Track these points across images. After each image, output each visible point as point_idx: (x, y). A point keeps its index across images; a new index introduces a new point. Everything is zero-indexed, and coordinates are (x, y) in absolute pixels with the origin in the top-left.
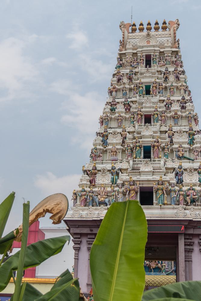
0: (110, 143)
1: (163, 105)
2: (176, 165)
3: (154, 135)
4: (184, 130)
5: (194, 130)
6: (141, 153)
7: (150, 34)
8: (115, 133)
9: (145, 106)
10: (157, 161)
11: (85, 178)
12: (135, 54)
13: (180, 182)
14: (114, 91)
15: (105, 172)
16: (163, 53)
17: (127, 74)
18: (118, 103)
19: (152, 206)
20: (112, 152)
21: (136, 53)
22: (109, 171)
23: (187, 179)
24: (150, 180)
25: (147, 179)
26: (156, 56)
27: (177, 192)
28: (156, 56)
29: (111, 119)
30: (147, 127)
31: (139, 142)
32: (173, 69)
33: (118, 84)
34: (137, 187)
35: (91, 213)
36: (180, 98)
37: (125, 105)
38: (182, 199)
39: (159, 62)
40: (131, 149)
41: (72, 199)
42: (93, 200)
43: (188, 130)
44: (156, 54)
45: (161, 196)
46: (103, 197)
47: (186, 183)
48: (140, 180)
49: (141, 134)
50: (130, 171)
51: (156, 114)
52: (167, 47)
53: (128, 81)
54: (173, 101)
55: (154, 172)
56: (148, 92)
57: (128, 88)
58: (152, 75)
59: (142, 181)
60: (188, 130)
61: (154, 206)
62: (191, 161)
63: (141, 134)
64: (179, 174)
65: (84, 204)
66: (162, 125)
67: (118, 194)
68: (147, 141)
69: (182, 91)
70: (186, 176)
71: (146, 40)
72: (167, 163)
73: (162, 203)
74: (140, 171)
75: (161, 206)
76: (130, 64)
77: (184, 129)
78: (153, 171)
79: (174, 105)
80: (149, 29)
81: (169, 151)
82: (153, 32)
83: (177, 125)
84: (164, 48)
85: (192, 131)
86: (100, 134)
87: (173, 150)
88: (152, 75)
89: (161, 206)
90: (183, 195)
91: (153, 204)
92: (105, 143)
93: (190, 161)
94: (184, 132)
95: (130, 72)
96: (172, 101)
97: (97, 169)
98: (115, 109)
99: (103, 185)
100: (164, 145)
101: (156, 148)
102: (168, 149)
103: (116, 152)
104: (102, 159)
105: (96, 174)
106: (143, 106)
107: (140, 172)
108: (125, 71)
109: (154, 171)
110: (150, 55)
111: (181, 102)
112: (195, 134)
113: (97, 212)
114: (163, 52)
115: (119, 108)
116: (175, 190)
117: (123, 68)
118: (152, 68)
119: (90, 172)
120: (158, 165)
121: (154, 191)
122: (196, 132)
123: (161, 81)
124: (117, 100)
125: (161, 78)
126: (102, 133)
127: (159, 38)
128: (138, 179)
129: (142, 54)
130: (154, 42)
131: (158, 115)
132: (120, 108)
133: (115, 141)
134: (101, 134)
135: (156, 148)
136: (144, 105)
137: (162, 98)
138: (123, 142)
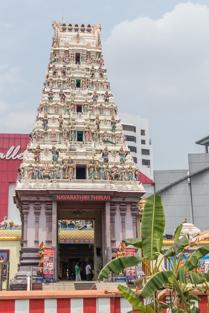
25: (82, 159)
43: (110, 119)
44: (84, 53)
52: (92, 48)
59: (79, 160)
60: (110, 119)
61: (87, 180)
68: (80, 127)
74: (76, 151)
93: (113, 144)
96: (98, 94)
103: (55, 135)
114: (89, 52)
120: (90, 147)
122: (117, 121)
124: (54, 91)
125: (88, 74)
126: (43, 118)
128: (75, 159)
136: (76, 96)
137: (90, 92)
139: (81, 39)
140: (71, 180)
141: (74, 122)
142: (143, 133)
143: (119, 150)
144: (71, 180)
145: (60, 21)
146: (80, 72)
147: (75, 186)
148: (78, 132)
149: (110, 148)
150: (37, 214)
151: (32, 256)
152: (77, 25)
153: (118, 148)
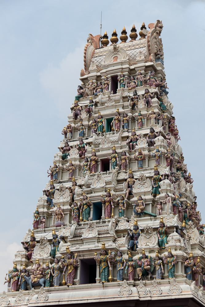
0: (55, 203)
1: (125, 143)
2: (130, 226)
3: (107, 186)
4: (147, 175)
5: (161, 173)
6: (89, 213)
7: (118, 47)
8: (61, 190)
9: (102, 148)
10: (107, 223)
11: (19, 254)
12: (98, 78)
13: (133, 248)
14: (68, 132)
15: (43, 243)
16: (134, 71)
17: (86, 106)
18: (72, 147)
19: (93, 284)
20: (56, 215)
21: (100, 76)
22: (50, 241)
23: (143, 243)
24: (92, 250)
25: (87, 249)
26: (124, 77)
27: (125, 262)
28: (124, 77)
29: (63, 169)
30: (98, 176)
31: (87, 198)
32: (143, 92)
33: (77, 121)
34: (77, 259)
35: (20, 300)
36: (148, 131)
37: (79, 149)
38: (130, 271)
39: (128, 84)
40: (78, 209)
41: (6, 282)
42: (26, 283)
43: (153, 174)
44: (124, 73)
45: (104, 270)
46: (36, 277)
47: (141, 249)
48: (79, 251)
49: (90, 187)
50: (71, 240)
51: (114, 157)
52: (139, 62)
53: (87, 115)
54: (139, 136)
55: (100, 238)
56: (110, 128)
57: (86, 125)
58: (115, 104)
59: (83, 251)
60: (153, 174)
61: (97, 284)
62: (153, 217)
63: (90, 187)
64: (133, 238)
65: (16, 287)
66: (120, 172)
67: (54, 273)
68: (98, 196)
69: (153, 121)
70: (142, 239)
71: (113, 56)
72: (119, 224)
73: (105, 279)
74: (82, 238)
75: (103, 283)
76: (92, 92)
77: (147, 174)
78: (98, 236)
79: (140, 143)
80: (115, 41)
81: (128, 207)
82: (120, 44)
83: (141, 169)
84: (135, 64)
85: (158, 175)
86: (46, 192)
87: (133, 204)
88: (115, 104)
89: (103, 283)
90: (132, 266)
91: (95, 282)
92: (50, 203)
93: (152, 217)
94: (147, 178)
95: (90, 103)
96: (138, 136)
97: (36, 240)
98: (68, 155)
99: (37, 261)
100: (119, 198)
101: (107, 204)
102: (124, 204)
103: (62, 214)
104: (45, 225)
105: (34, 246)
106: (99, 148)
107: (82, 239)
108: (85, 102)
109: (100, 237)
110: (117, 76)
111: (149, 136)
112: (162, 179)
113: (27, 298)
114: (134, 69)
115: (72, 155)
116: (121, 260)
117: (83, 98)
118: (117, 94)
119: (28, 244)
120: (106, 228)
121: (97, 264)
122: (163, 177)
123: (128, 110)
124: (71, 144)
125: (127, 106)
126: (48, 191)
127: (131, 50)
128: (77, 250)
129: (107, 76)
130: (123, 57)
131: (116, 158)
132: (74, 154)
133: (143, 190)
134: (47, 192)
135: (107, 205)
136: (101, 146)
137: (126, 134)
138: (73, 199)
139: (121, 52)
140: (68, 286)
141: (90, 189)
143: (52, 238)
144: (68, 286)
145: (97, 33)
146: (112, 105)
147: (72, 297)
148: (94, 204)
149: (144, 223)
152: (115, 34)
153: (156, 224)
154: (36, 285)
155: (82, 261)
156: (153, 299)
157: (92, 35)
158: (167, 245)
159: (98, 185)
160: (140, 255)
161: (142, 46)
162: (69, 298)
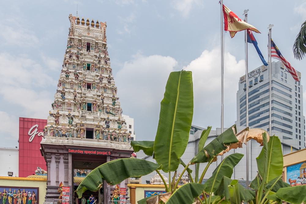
18: (71, 72)
34: (84, 127)
43: (112, 97)
44: (93, 43)
56: (88, 68)
59: (88, 124)
61: (94, 139)
94: (110, 97)
110: (90, 43)
123: (97, 62)
136: (87, 76)
141: (85, 96)
142: (130, 127)
148: (88, 103)
150: (58, 162)
151: (54, 192)
154: (63, 135)
155: (87, 128)
156: (120, 149)
157: (268, 55)
158: (122, 128)
159: (89, 95)
160: (50, 125)
161: (97, 32)
162: (83, 143)
